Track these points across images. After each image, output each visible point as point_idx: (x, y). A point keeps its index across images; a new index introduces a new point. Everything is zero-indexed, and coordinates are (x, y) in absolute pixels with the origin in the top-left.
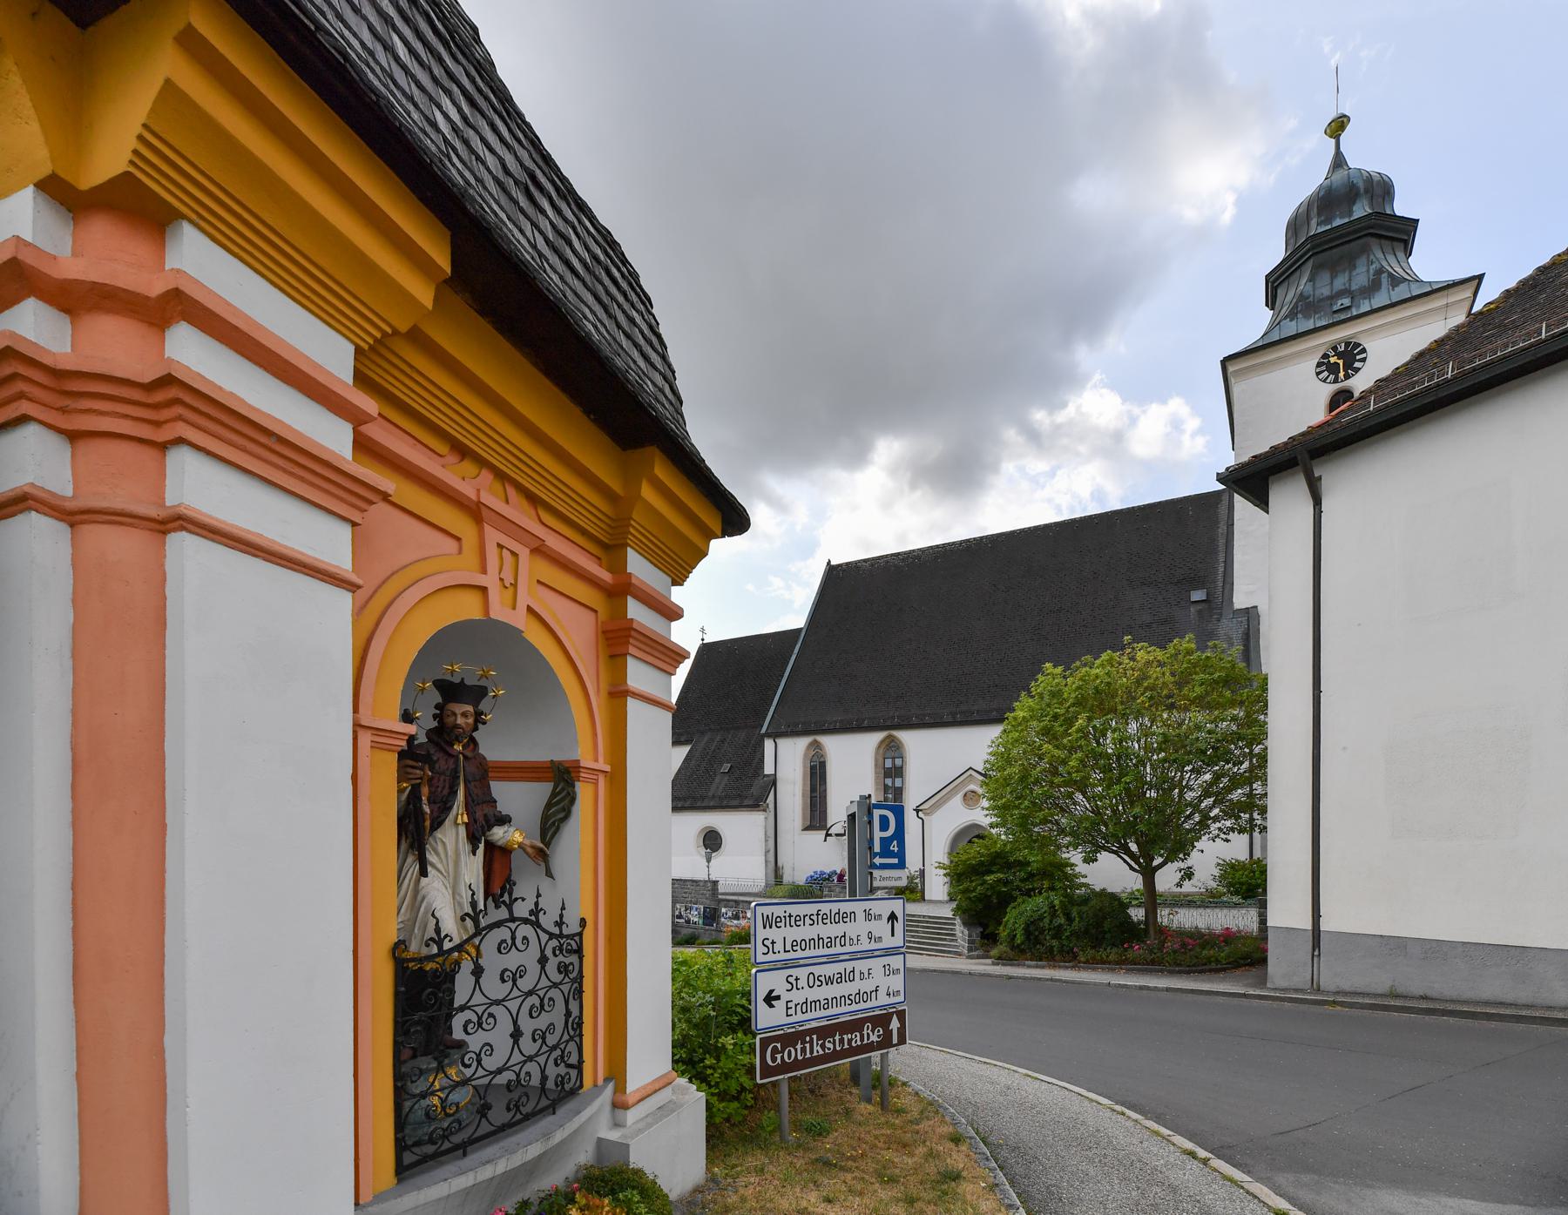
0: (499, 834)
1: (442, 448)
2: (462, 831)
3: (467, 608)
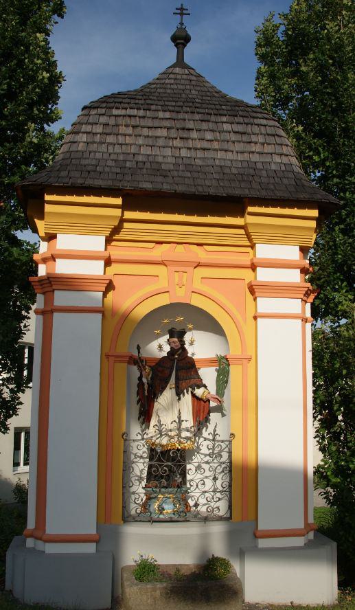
0: (199, 392)
1: (152, 245)
2: (174, 391)
3: (164, 300)
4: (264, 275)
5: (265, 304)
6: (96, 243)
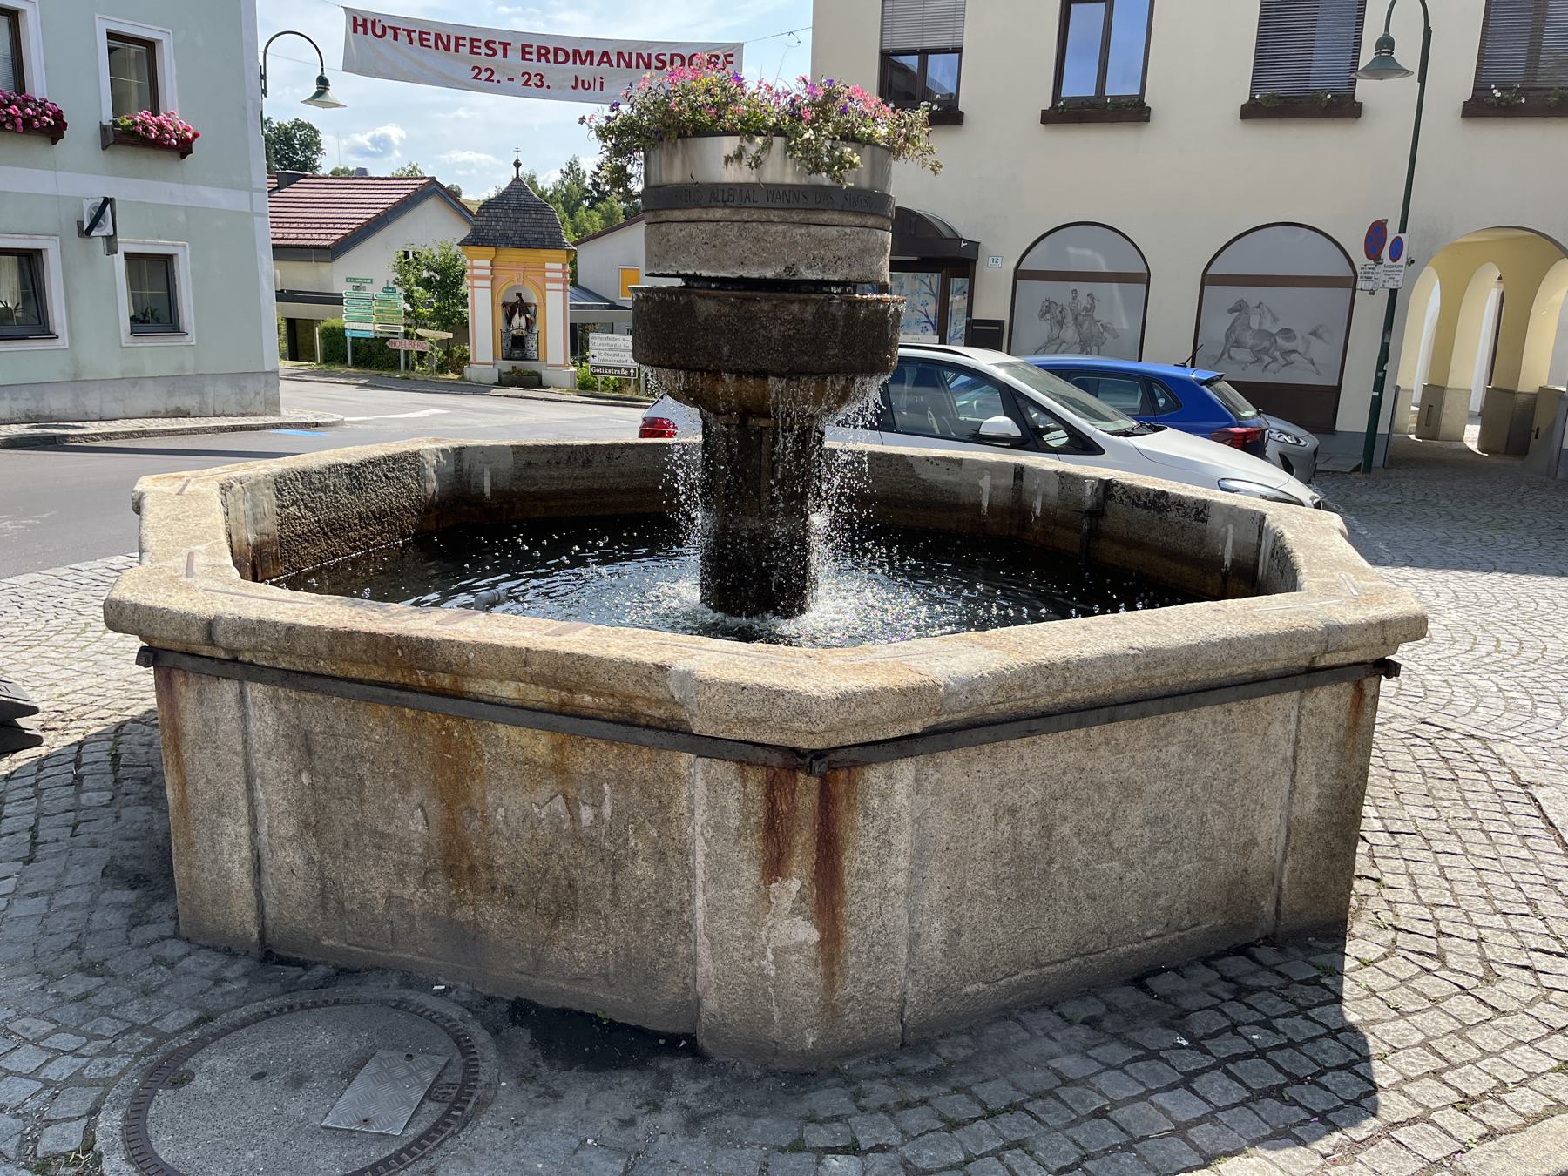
5: (549, 286)
6: (488, 263)
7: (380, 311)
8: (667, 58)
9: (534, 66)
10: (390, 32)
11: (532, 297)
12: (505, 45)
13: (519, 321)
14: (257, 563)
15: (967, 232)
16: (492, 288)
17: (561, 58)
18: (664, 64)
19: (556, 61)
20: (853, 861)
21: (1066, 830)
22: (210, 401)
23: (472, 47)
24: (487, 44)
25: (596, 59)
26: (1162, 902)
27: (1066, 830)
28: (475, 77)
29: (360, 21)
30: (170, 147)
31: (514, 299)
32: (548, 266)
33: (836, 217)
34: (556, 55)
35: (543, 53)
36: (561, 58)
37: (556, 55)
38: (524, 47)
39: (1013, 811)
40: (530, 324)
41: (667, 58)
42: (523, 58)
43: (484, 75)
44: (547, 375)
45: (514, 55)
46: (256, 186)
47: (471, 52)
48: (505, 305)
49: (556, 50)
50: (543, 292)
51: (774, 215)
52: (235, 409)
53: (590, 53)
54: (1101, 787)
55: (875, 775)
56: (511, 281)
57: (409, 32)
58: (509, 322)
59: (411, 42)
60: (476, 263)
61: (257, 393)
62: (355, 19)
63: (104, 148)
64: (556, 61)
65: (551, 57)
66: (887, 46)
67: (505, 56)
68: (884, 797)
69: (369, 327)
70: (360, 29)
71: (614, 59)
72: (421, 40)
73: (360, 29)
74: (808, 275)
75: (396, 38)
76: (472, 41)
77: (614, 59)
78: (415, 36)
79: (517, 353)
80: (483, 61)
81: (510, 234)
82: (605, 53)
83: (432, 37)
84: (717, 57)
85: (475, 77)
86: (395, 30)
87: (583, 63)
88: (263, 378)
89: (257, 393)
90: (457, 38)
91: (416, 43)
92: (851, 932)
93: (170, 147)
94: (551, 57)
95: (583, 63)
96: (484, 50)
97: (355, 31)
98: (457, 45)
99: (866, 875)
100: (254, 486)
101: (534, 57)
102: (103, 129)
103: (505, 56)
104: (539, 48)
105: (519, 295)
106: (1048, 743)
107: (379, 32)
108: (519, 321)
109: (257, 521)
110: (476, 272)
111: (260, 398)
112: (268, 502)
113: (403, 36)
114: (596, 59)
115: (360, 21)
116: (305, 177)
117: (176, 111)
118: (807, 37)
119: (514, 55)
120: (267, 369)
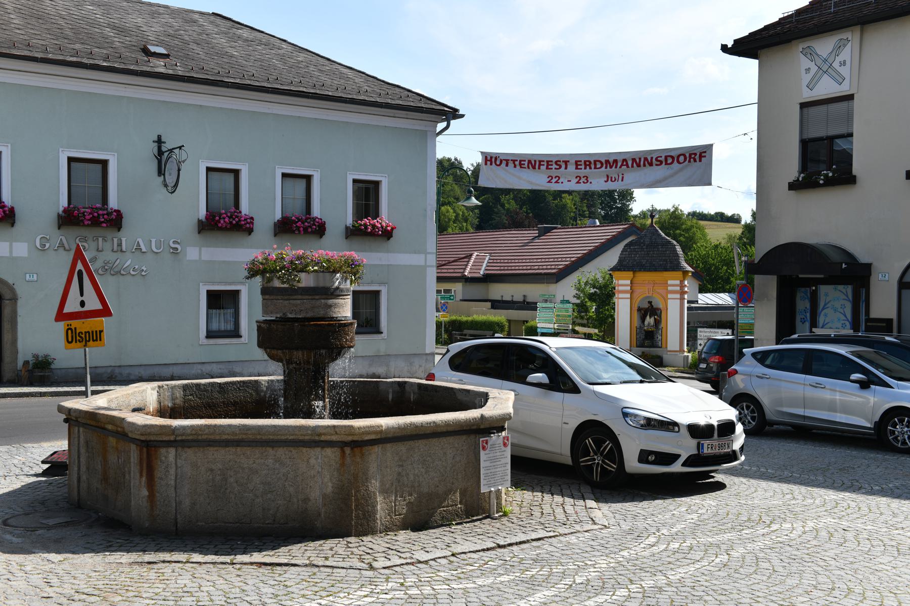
4: (669, 288)
5: (670, 296)
6: (629, 282)
7: (558, 315)
8: (663, 159)
9: (583, 172)
10: (504, 163)
11: (658, 303)
12: (566, 162)
13: (650, 320)
14: (161, 412)
15: (863, 259)
16: (631, 298)
17: (599, 165)
18: (661, 162)
19: (595, 168)
20: (158, 474)
21: (232, 480)
22: (393, 370)
23: (548, 165)
24: (556, 163)
25: (619, 164)
26: (271, 512)
27: (232, 480)
28: (549, 182)
29: (489, 158)
30: (378, 235)
31: (646, 306)
32: (670, 282)
33: (300, 297)
34: (595, 165)
35: (587, 164)
36: (599, 165)
37: (595, 165)
38: (576, 162)
39: (212, 470)
40: (657, 323)
41: (663, 159)
42: (577, 168)
43: (554, 180)
44: (666, 358)
45: (571, 167)
46: (429, 251)
47: (547, 168)
48: (639, 310)
49: (595, 162)
50: (666, 300)
51: (279, 297)
52: (409, 375)
53: (615, 161)
54: (243, 469)
55: (163, 451)
56: (643, 292)
57: (514, 161)
58: (643, 321)
59: (515, 166)
60: (621, 282)
61: (420, 366)
62: (486, 157)
63: (346, 238)
64: (595, 168)
65: (593, 166)
66: (805, 137)
67: (566, 168)
68: (166, 457)
69: (551, 326)
70: (489, 163)
71: (630, 163)
72: (520, 164)
73: (489, 163)
74: (290, 316)
75: (507, 165)
76: (548, 162)
77: (630, 163)
78: (517, 163)
79: (647, 343)
80: (554, 173)
81: (644, 262)
82: (625, 160)
83: (526, 163)
84: (695, 154)
85: (549, 182)
86: (507, 161)
87: (611, 167)
88: (425, 357)
89: (420, 366)
90: (540, 162)
91: (518, 167)
92: (158, 495)
93: (378, 235)
94: (593, 166)
95: (611, 167)
96: (555, 166)
97: (486, 164)
98: (540, 165)
99: (161, 479)
100: (173, 387)
101: (583, 167)
102: (347, 228)
103: (566, 168)
104: (585, 162)
105: (650, 303)
106: (222, 451)
107: (498, 163)
108: (650, 320)
109: (173, 399)
110: (621, 288)
111: (422, 369)
112: (179, 394)
113: (511, 164)
114: (619, 164)
115: (489, 158)
116: (555, 228)
117: (385, 218)
118: (755, 135)
119: (571, 167)
120: (427, 352)
